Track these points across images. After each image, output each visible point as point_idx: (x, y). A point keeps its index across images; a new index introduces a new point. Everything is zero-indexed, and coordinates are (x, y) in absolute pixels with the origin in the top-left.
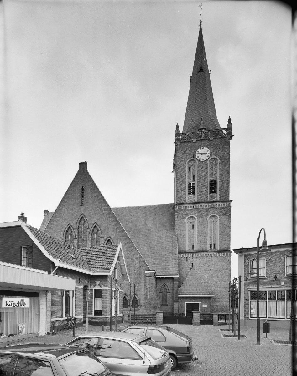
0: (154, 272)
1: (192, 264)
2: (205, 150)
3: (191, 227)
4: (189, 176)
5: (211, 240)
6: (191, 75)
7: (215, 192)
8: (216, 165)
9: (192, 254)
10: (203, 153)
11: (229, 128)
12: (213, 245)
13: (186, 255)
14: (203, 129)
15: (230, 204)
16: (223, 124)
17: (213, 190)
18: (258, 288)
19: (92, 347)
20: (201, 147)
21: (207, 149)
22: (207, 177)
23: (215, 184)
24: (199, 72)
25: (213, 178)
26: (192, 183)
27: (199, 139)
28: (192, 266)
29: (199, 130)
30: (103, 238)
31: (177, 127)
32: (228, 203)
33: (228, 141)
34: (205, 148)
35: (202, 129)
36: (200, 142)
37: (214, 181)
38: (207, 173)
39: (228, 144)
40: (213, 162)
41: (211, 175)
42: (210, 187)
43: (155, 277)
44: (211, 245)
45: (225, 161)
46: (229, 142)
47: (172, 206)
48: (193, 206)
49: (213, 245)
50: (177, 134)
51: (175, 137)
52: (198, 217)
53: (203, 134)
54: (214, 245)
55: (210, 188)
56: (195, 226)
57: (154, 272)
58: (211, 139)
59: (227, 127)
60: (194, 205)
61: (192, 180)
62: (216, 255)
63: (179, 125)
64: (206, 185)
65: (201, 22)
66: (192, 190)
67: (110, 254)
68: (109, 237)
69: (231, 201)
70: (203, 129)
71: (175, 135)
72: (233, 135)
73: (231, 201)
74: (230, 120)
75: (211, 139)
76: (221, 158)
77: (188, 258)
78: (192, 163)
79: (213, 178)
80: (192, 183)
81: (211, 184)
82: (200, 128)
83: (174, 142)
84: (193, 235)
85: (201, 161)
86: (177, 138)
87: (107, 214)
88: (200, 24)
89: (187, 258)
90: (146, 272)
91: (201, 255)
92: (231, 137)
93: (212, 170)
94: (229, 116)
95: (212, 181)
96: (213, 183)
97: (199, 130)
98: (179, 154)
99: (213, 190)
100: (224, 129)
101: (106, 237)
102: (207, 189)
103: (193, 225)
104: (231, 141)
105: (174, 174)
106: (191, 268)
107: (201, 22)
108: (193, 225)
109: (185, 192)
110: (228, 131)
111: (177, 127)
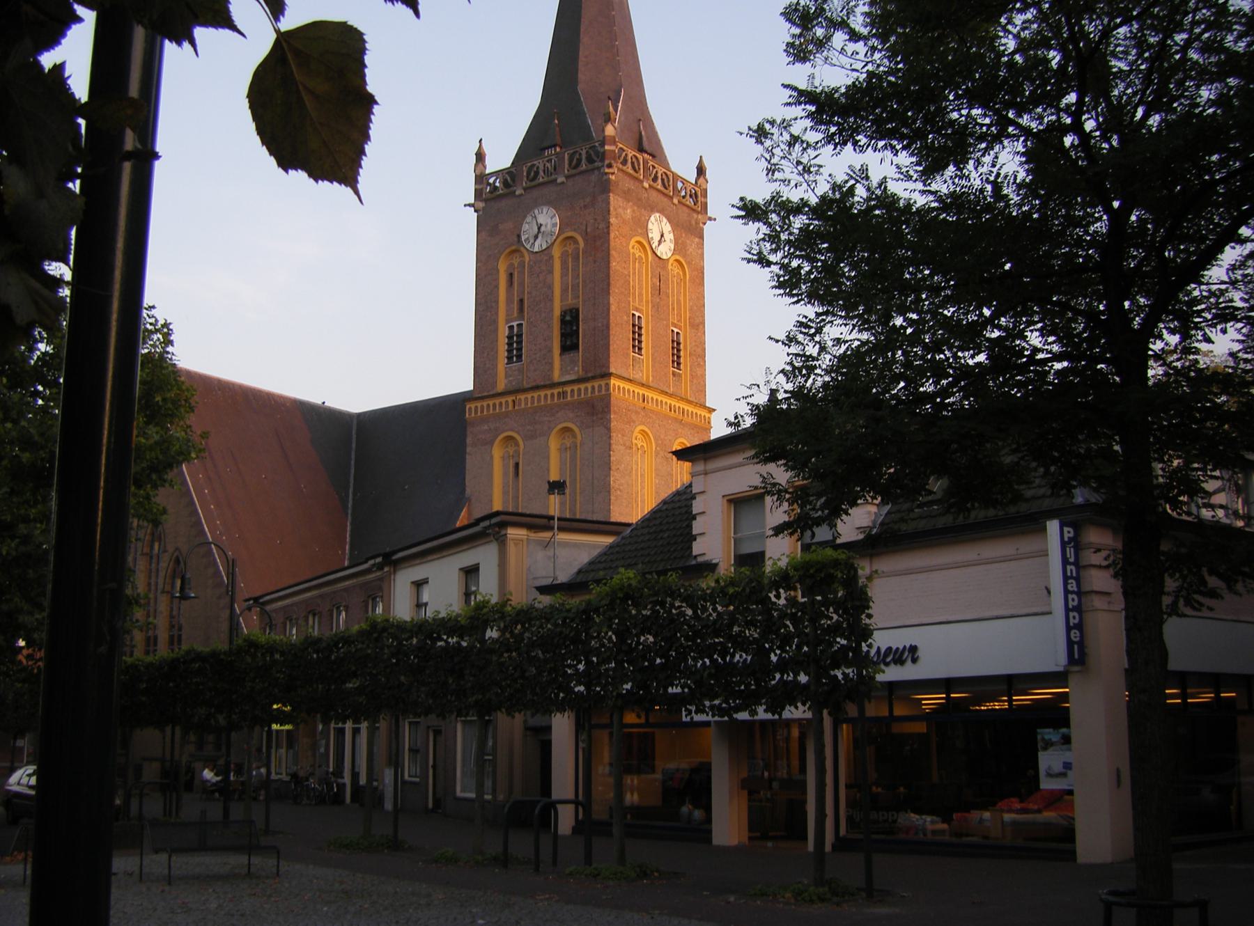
3: (511, 469)
7: (575, 347)
17: (570, 343)
18: (891, 710)
19: (1170, 615)
32: (603, 383)
38: (551, 287)
40: (570, 248)
41: (564, 291)
50: (481, 178)
52: (525, 438)
58: (559, 180)
64: (550, 327)
75: (559, 180)
76: (585, 235)
79: (570, 301)
80: (515, 324)
81: (563, 322)
93: (567, 275)
102: (550, 338)
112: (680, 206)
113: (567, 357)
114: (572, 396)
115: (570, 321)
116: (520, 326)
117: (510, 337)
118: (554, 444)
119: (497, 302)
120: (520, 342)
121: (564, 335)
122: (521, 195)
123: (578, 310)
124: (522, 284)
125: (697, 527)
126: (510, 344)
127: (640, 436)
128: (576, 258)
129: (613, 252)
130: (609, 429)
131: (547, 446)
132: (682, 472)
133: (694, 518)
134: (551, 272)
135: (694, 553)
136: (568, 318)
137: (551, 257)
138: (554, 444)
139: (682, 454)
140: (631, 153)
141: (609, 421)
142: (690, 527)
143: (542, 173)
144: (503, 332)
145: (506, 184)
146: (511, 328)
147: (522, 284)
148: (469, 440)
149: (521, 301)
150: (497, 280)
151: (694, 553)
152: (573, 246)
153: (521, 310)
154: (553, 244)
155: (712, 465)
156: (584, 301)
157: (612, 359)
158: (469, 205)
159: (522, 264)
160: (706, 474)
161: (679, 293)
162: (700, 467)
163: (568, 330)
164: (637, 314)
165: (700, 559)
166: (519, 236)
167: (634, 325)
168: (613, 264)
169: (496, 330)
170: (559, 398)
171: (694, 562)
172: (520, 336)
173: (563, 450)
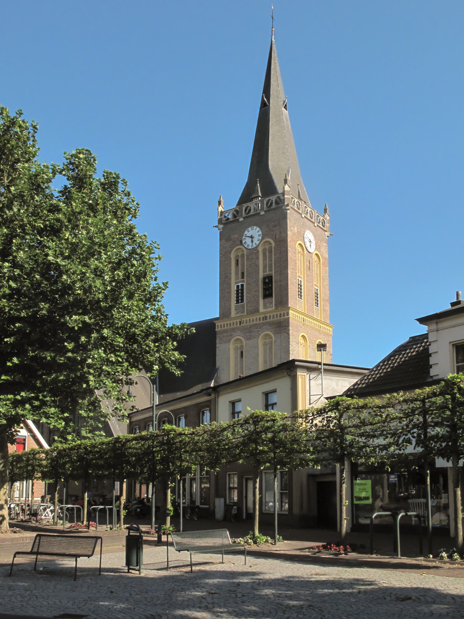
7: (270, 295)
17: (268, 294)
38: (258, 266)
41: (265, 267)
64: (258, 285)
79: (268, 273)
80: (240, 284)
81: (265, 283)
93: (266, 260)
96: (267, 280)
102: (258, 291)
112: (318, 227)
113: (267, 300)
114: (270, 319)
115: (268, 283)
116: (242, 285)
117: (237, 291)
118: (260, 342)
119: (230, 274)
120: (242, 293)
121: (265, 290)
122: (263, 215)
123: (272, 277)
124: (243, 265)
125: (432, 360)
126: (237, 294)
127: (302, 338)
128: (270, 252)
129: (289, 248)
130: (289, 334)
131: (258, 344)
132: (423, 329)
133: (430, 355)
134: (258, 258)
135: (431, 375)
136: (267, 280)
137: (258, 251)
138: (260, 342)
139: (422, 321)
140: (296, 200)
141: (289, 330)
142: (428, 361)
143: (274, 204)
144: (234, 288)
145: (234, 216)
146: (238, 286)
147: (243, 265)
148: (217, 341)
149: (243, 273)
150: (230, 263)
151: (431, 375)
152: (269, 246)
153: (243, 277)
154: (259, 244)
155: (441, 325)
156: (275, 273)
157: (289, 300)
158: (216, 227)
159: (243, 256)
160: (437, 331)
161: (317, 270)
162: (434, 327)
163: (267, 286)
164: (300, 279)
165: (435, 378)
166: (241, 242)
167: (299, 285)
168: (289, 254)
169: (230, 288)
170: (263, 320)
171: (431, 380)
172: (242, 290)
173: (265, 344)
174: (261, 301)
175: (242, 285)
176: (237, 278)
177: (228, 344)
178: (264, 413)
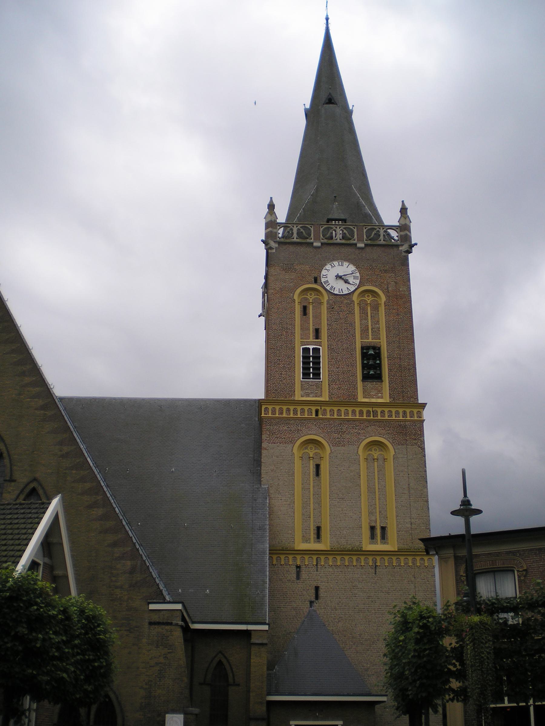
0: (179, 607)
1: (317, 589)
2: (346, 268)
4: (304, 329)
5: (371, 513)
6: (308, 106)
7: (378, 377)
8: (376, 308)
9: (315, 557)
10: (339, 276)
11: (404, 228)
12: (378, 531)
13: (295, 559)
14: (339, 220)
15: (420, 414)
16: (389, 216)
20: (334, 260)
21: (352, 268)
22: (354, 336)
23: (378, 355)
24: (327, 103)
25: (370, 340)
26: (311, 347)
27: (331, 242)
28: (317, 597)
29: (329, 220)
30: (13, 484)
31: (271, 206)
32: (415, 411)
33: (404, 254)
34: (346, 264)
35: (335, 220)
36: (332, 249)
37: (374, 348)
38: (352, 325)
39: (405, 263)
40: (369, 299)
41: (364, 331)
42: (363, 364)
43: (186, 629)
44: (373, 528)
45: (401, 301)
46: (407, 259)
47: (260, 402)
48: (317, 412)
49: (378, 531)
50: (271, 224)
51: (266, 229)
53: (339, 231)
54: (383, 529)
55: (364, 366)
56: (322, 467)
57: (179, 607)
59: (398, 224)
60: (319, 408)
61: (311, 339)
62: (391, 562)
63: (407, 205)
65: (327, 19)
66: (311, 365)
67: (16, 531)
68: (35, 479)
69: (423, 406)
70: (339, 220)
71: (266, 224)
72: (416, 244)
73: (423, 406)
74: (404, 210)
77: (303, 568)
78: (311, 297)
79: (370, 340)
80: (311, 347)
81: (365, 355)
82: (330, 217)
83: (262, 241)
84: (318, 495)
85: (337, 295)
86: (271, 232)
87: (36, 409)
88: (325, 22)
89: (298, 567)
90: (152, 607)
91: (414, 561)
92: (411, 246)
93: (366, 319)
94: (403, 201)
95: (368, 348)
96: (371, 352)
97: (329, 220)
98: (272, 270)
99: (372, 372)
100: (391, 227)
101: (25, 480)
102: (354, 365)
103: (318, 467)
104: (410, 256)
105: (263, 319)
106: (311, 603)
107: (327, 19)
108: (318, 467)
109: (292, 368)
110: (402, 233)
111: (271, 206)
124: (318, 317)
172: (317, 358)
174: (360, 384)
175: (316, 350)
176: (304, 335)
177: (290, 446)
178: (41, 569)
